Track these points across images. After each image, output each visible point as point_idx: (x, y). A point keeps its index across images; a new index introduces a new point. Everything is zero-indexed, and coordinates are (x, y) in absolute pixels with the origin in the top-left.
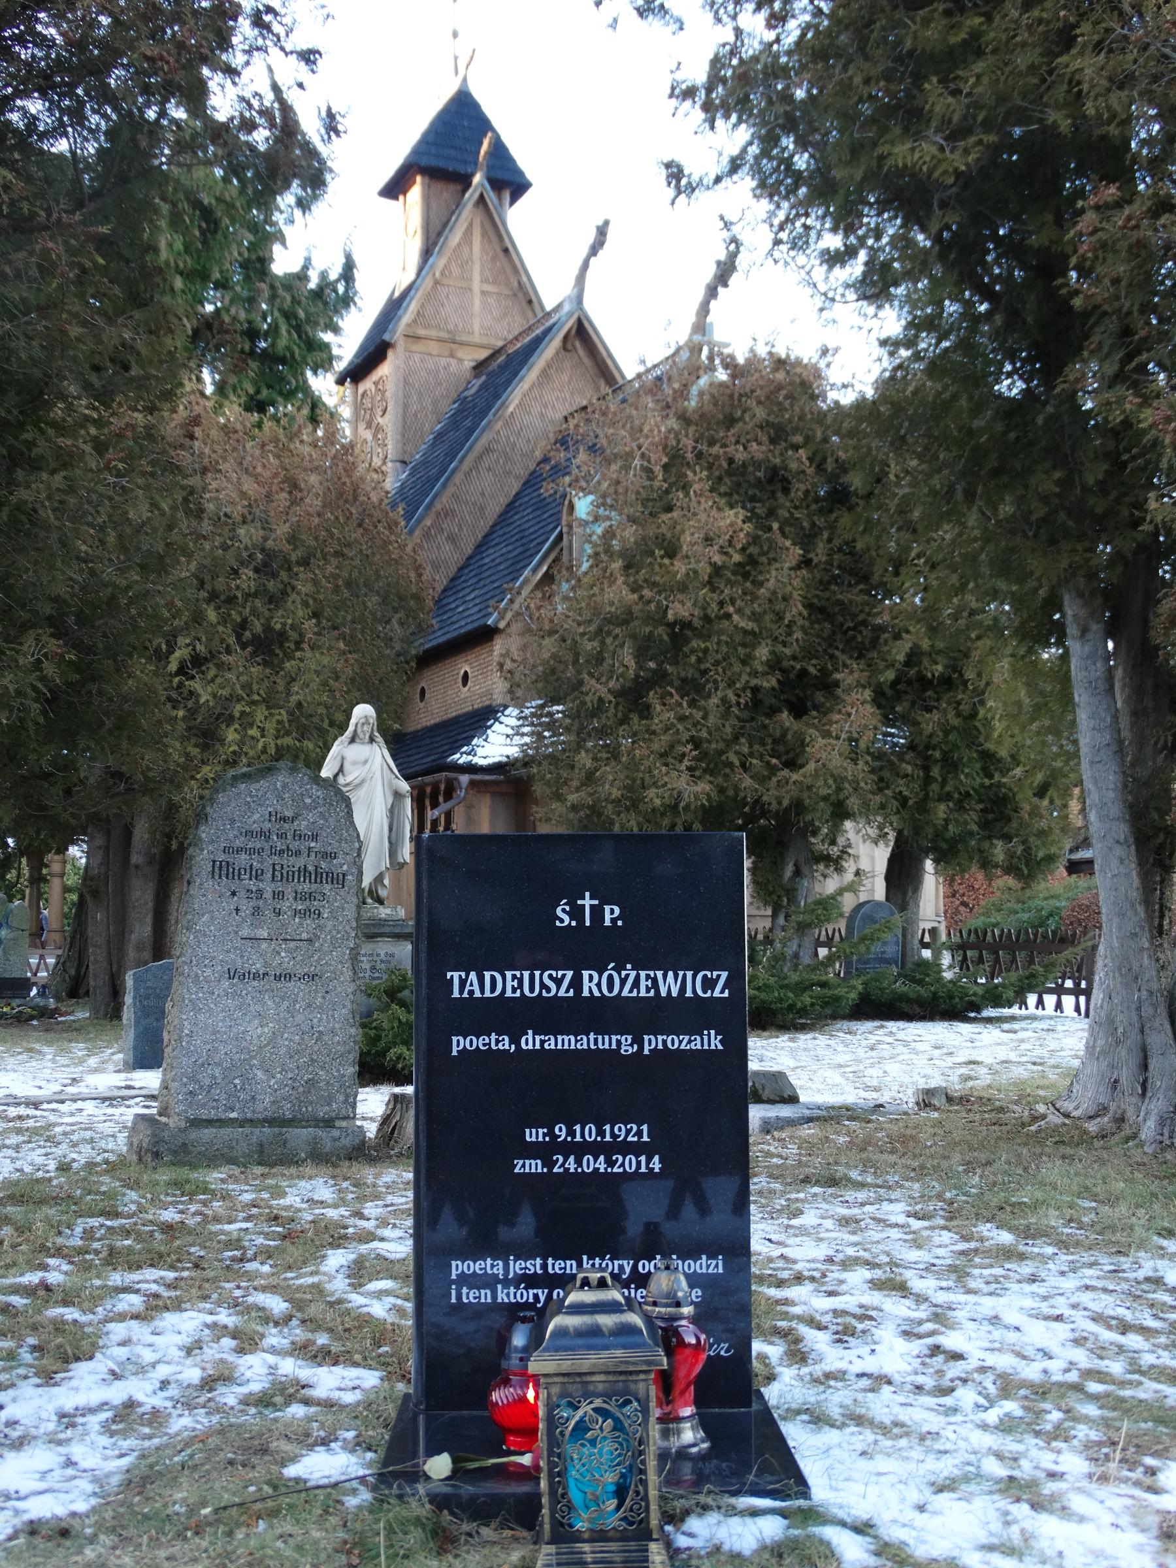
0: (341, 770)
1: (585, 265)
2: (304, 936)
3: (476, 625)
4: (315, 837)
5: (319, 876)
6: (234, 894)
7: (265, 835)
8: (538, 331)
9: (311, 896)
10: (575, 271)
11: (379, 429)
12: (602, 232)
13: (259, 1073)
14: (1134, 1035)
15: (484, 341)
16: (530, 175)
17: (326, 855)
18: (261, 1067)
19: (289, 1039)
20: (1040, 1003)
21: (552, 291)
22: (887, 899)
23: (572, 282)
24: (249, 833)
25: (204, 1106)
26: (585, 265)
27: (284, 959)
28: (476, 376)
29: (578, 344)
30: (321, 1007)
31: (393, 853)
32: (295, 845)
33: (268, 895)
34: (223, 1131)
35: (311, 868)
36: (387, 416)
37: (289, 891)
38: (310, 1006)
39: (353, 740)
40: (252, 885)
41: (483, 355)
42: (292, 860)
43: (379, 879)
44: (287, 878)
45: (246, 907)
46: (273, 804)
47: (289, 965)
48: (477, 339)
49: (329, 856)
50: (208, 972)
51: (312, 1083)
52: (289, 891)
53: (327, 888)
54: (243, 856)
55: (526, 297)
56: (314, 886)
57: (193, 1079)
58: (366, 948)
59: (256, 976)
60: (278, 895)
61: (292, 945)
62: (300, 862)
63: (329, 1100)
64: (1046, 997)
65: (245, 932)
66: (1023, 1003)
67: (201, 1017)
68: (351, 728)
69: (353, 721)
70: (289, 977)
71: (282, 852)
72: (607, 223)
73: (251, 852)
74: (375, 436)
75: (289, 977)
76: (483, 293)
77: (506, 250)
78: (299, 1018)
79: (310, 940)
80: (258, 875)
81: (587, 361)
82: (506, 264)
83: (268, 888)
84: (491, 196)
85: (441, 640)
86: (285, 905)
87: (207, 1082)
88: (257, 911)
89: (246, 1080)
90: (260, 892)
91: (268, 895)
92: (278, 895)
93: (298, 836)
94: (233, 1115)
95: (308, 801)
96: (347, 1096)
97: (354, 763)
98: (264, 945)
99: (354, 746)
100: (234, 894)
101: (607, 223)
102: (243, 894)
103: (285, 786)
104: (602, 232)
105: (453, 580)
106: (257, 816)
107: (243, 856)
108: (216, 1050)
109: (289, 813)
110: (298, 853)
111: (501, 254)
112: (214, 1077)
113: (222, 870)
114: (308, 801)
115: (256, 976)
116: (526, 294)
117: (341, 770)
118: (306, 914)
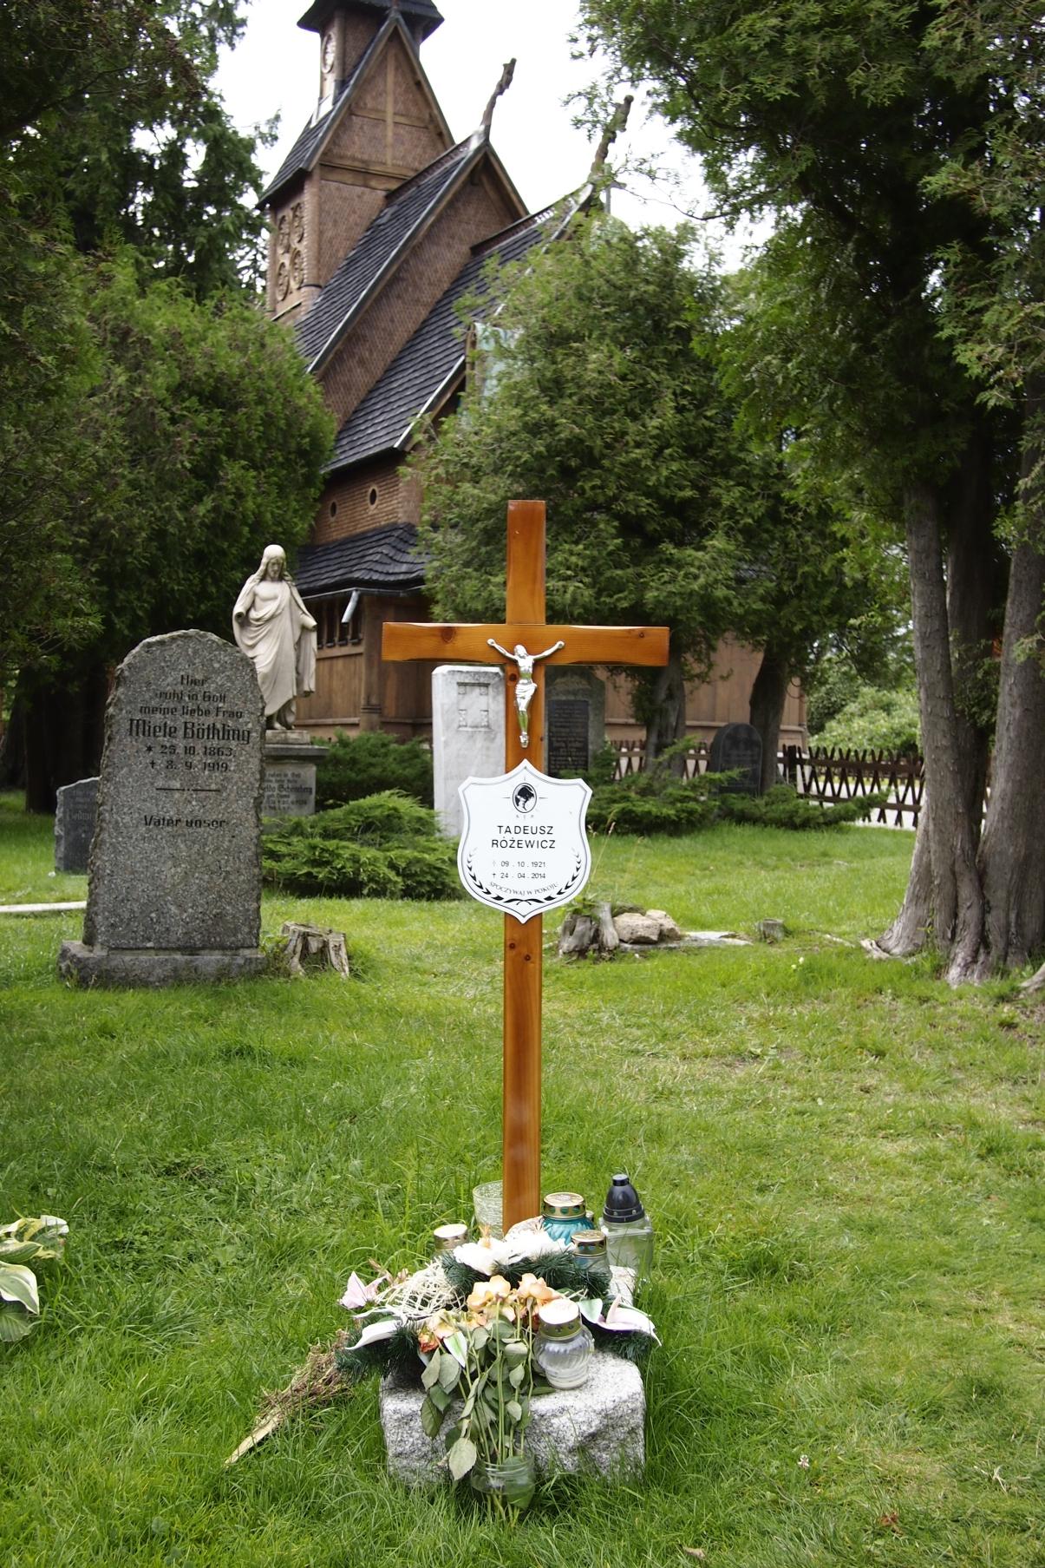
0: (253, 605)
1: (492, 104)
2: (213, 787)
3: (383, 447)
4: (223, 698)
5: (226, 733)
6: (150, 749)
7: (178, 697)
8: (448, 165)
9: (219, 751)
10: (484, 108)
11: (298, 254)
12: (509, 69)
13: (173, 908)
14: (948, 887)
15: (396, 171)
16: (441, 10)
17: (232, 714)
18: (174, 903)
19: (200, 879)
20: (882, 816)
21: (462, 125)
22: (752, 721)
23: (481, 118)
24: (163, 695)
25: (123, 937)
26: (492, 104)
27: (194, 808)
28: (388, 206)
29: (485, 180)
30: (228, 850)
31: (299, 682)
32: (205, 706)
33: (180, 750)
34: (143, 958)
35: (219, 726)
36: (305, 243)
37: (200, 750)
38: (217, 849)
39: (263, 579)
40: (166, 741)
41: (394, 185)
42: (202, 718)
43: (286, 707)
44: (197, 735)
45: (161, 762)
46: (184, 668)
47: (199, 814)
48: (390, 170)
49: (236, 715)
50: (127, 819)
51: (219, 917)
52: (200, 750)
53: (233, 744)
54: (158, 715)
55: (437, 129)
56: (222, 742)
57: (114, 913)
58: (270, 771)
59: (170, 822)
60: (190, 751)
61: (202, 794)
62: (209, 720)
63: (236, 931)
64: (888, 812)
65: (160, 784)
66: (867, 816)
67: (121, 858)
68: (262, 567)
69: (264, 560)
70: (199, 823)
71: (193, 711)
72: (514, 61)
73: (164, 711)
74: (293, 263)
75: (199, 823)
76: (396, 123)
77: (418, 84)
78: (209, 859)
79: (218, 790)
80: (172, 732)
81: (492, 194)
82: (419, 97)
83: (180, 744)
84: (404, 31)
85: (351, 460)
86: (195, 760)
87: (126, 915)
88: (170, 764)
89: (160, 913)
90: (173, 747)
91: (180, 750)
92: (190, 751)
93: (207, 697)
94: (150, 945)
95: (216, 665)
96: (251, 928)
97: (265, 600)
98: (177, 795)
99: (263, 584)
100: (150, 749)
101: (514, 61)
102: (158, 749)
103: (196, 652)
104: (509, 69)
105: (363, 402)
106: (170, 680)
107: (158, 715)
108: (135, 887)
109: (199, 677)
110: (207, 713)
111: (414, 88)
112: (132, 911)
113: (139, 728)
114: (216, 665)
115: (170, 822)
116: (437, 126)
117: (253, 605)
118: (214, 767)
